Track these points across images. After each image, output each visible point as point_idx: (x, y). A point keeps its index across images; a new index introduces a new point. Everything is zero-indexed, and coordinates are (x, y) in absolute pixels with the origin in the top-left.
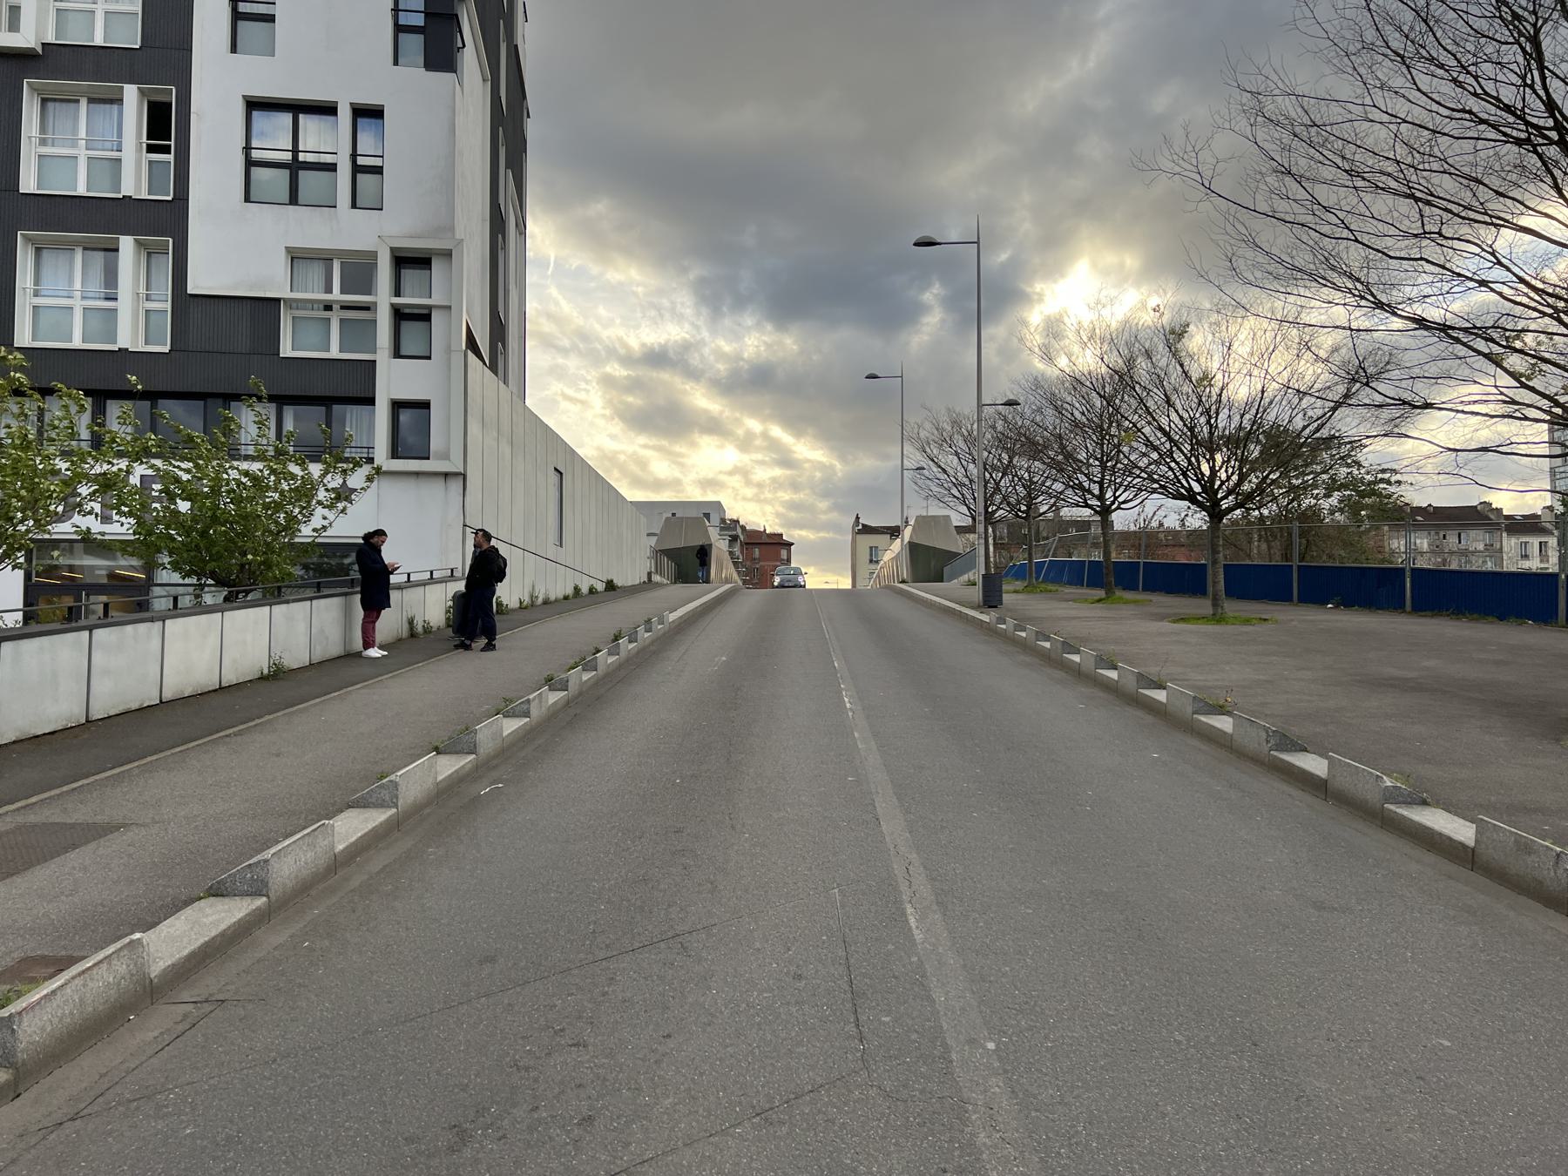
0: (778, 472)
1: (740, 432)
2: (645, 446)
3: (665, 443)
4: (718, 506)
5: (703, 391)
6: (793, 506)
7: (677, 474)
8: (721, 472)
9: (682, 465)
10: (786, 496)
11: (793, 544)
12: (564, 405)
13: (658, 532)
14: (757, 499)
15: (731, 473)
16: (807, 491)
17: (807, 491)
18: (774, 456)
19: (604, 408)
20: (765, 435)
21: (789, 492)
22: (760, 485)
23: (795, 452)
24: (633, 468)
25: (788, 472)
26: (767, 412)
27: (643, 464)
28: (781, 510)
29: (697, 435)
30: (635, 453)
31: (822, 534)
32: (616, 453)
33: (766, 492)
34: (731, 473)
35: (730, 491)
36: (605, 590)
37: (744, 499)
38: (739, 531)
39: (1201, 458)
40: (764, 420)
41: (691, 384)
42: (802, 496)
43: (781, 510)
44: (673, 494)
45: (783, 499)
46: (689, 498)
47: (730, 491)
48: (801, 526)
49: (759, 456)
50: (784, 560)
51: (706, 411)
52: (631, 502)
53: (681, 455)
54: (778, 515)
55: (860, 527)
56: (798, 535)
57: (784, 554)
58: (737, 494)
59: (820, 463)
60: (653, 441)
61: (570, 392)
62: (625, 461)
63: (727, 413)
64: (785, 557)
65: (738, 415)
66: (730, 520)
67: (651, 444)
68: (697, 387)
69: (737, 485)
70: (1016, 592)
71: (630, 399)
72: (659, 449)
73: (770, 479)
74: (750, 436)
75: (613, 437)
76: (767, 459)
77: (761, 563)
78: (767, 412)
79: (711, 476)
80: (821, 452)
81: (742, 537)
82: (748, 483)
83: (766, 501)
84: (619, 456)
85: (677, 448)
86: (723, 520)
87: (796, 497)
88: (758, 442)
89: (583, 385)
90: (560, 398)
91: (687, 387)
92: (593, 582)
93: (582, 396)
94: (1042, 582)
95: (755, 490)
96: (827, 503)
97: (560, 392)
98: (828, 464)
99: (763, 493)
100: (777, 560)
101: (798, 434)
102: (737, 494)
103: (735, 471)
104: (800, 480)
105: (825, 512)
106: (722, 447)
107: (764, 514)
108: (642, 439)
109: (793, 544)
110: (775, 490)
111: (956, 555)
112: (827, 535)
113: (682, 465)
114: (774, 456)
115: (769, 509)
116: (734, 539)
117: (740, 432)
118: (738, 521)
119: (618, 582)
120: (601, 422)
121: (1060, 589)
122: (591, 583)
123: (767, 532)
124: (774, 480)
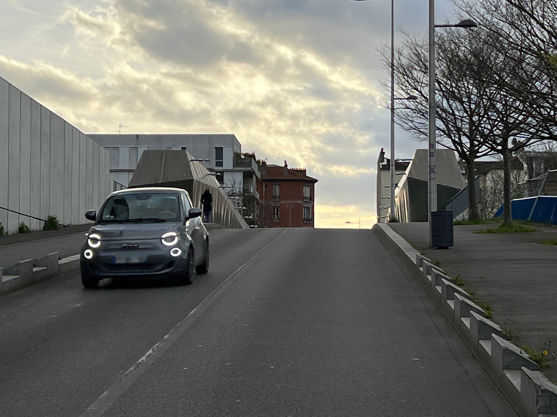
0: (313, 103)
1: (272, 58)
2: (169, 75)
3: (189, 71)
4: (232, 139)
5: (231, 15)
6: (329, 139)
7: (204, 104)
8: (251, 103)
9: (208, 95)
10: (322, 129)
11: (316, 181)
12: (81, 30)
13: (413, 158)
14: (292, 133)
15: (263, 105)
16: (345, 124)
17: (345, 124)
18: (308, 86)
19: (123, 33)
20: (298, 63)
21: (326, 125)
22: (294, 117)
23: (331, 81)
24: (157, 98)
25: (324, 103)
26: (299, 38)
27: (167, 94)
28: (317, 143)
29: (225, 63)
30: (158, 82)
31: (362, 170)
32: (138, 81)
33: (301, 126)
34: (263, 105)
35: (263, 123)
36: (44, 229)
37: (278, 132)
38: (255, 167)
39: (477, 109)
40: (297, 45)
41: (217, 8)
42: (340, 129)
43: (317, 143)
44: (201, 126)
45: (319, 132)
46: (216, 130)
47: (263, 123)
48: (339, 162)
49: (291, 86)
50: (306, 198)
51: (234, 37)
52: (93, 137)
53: (207, 84)
54: (313, 149)
55: (385, 163)
56: (336, 171)
57: (306, 191)
58: (270, 127)
59: (358, 92)
60: (177, 70)
61: (86, 16)
62: (148, 90)
63: (257, 38)
64: (308, 195)
65: (267, 41)
66: (246, 155)
67: (175, 72)
68: (224, 11)
69: (268, 116)
70: (490, 232)
71: (151, 23)
72: (178, 77)
73: (304, 110)
74: (282, 63)
75: (133, 65)
76: (301, 89)
77: (282, 202)
78: (299, 38)
79: (241, 106)
80: (355, 82)
81: (258, 174)
82: (281, 114)
83: (302, 135)
84: (141, 85)
85: (203, 77)
86: (237, 156)
87: (333, 130)
88: (291, 71)
89: (99, 9)
90: (75, 23)
91: (214, 11)
92: (22, 219)
93: (100, 20)
94: (529, 222)
95: (289, 123)
96: (367, 137)
97: (75, 16)
98: (367, 94)
99: (298, 126)
100: (299, 199)
101: (334, 62)
102: (270, 127)
103: (267, 102)
104: (338, 111)
105: (365, 147)
106: (250, 76)
107: (299, 149)
108: (165, 68)
109: (316, 181)
110: (311, 122)
111: (457, 190)
112: (367, 171)
113: (208, 95)
114: (308, 86)
115: (305, 143)
116: (248, 176)
117: (272, 58)
118: (253, 156)
119: (61, 220)
120: (120, 49)
121: (538, 229)
122: (21, 221)
123: (289, 168)
124: (309, 111)
